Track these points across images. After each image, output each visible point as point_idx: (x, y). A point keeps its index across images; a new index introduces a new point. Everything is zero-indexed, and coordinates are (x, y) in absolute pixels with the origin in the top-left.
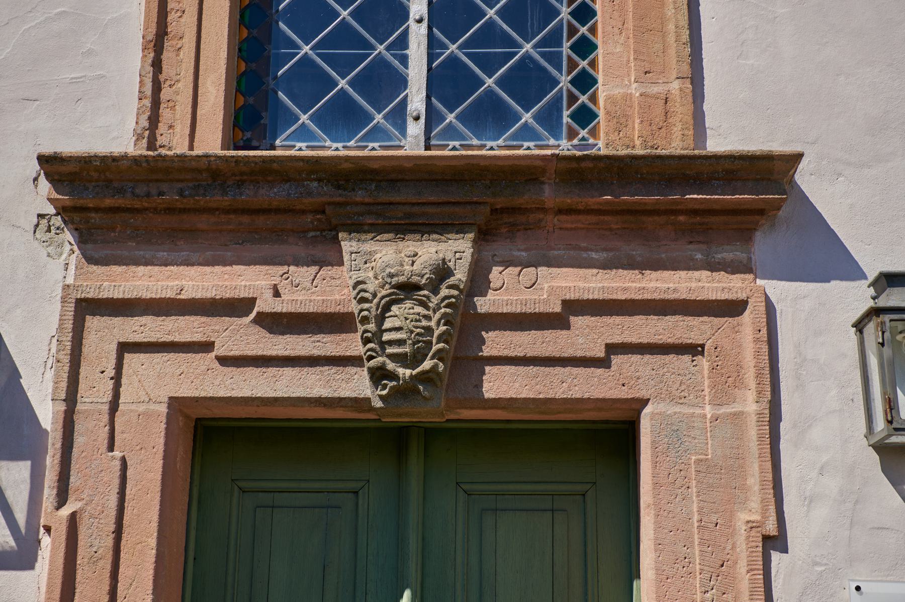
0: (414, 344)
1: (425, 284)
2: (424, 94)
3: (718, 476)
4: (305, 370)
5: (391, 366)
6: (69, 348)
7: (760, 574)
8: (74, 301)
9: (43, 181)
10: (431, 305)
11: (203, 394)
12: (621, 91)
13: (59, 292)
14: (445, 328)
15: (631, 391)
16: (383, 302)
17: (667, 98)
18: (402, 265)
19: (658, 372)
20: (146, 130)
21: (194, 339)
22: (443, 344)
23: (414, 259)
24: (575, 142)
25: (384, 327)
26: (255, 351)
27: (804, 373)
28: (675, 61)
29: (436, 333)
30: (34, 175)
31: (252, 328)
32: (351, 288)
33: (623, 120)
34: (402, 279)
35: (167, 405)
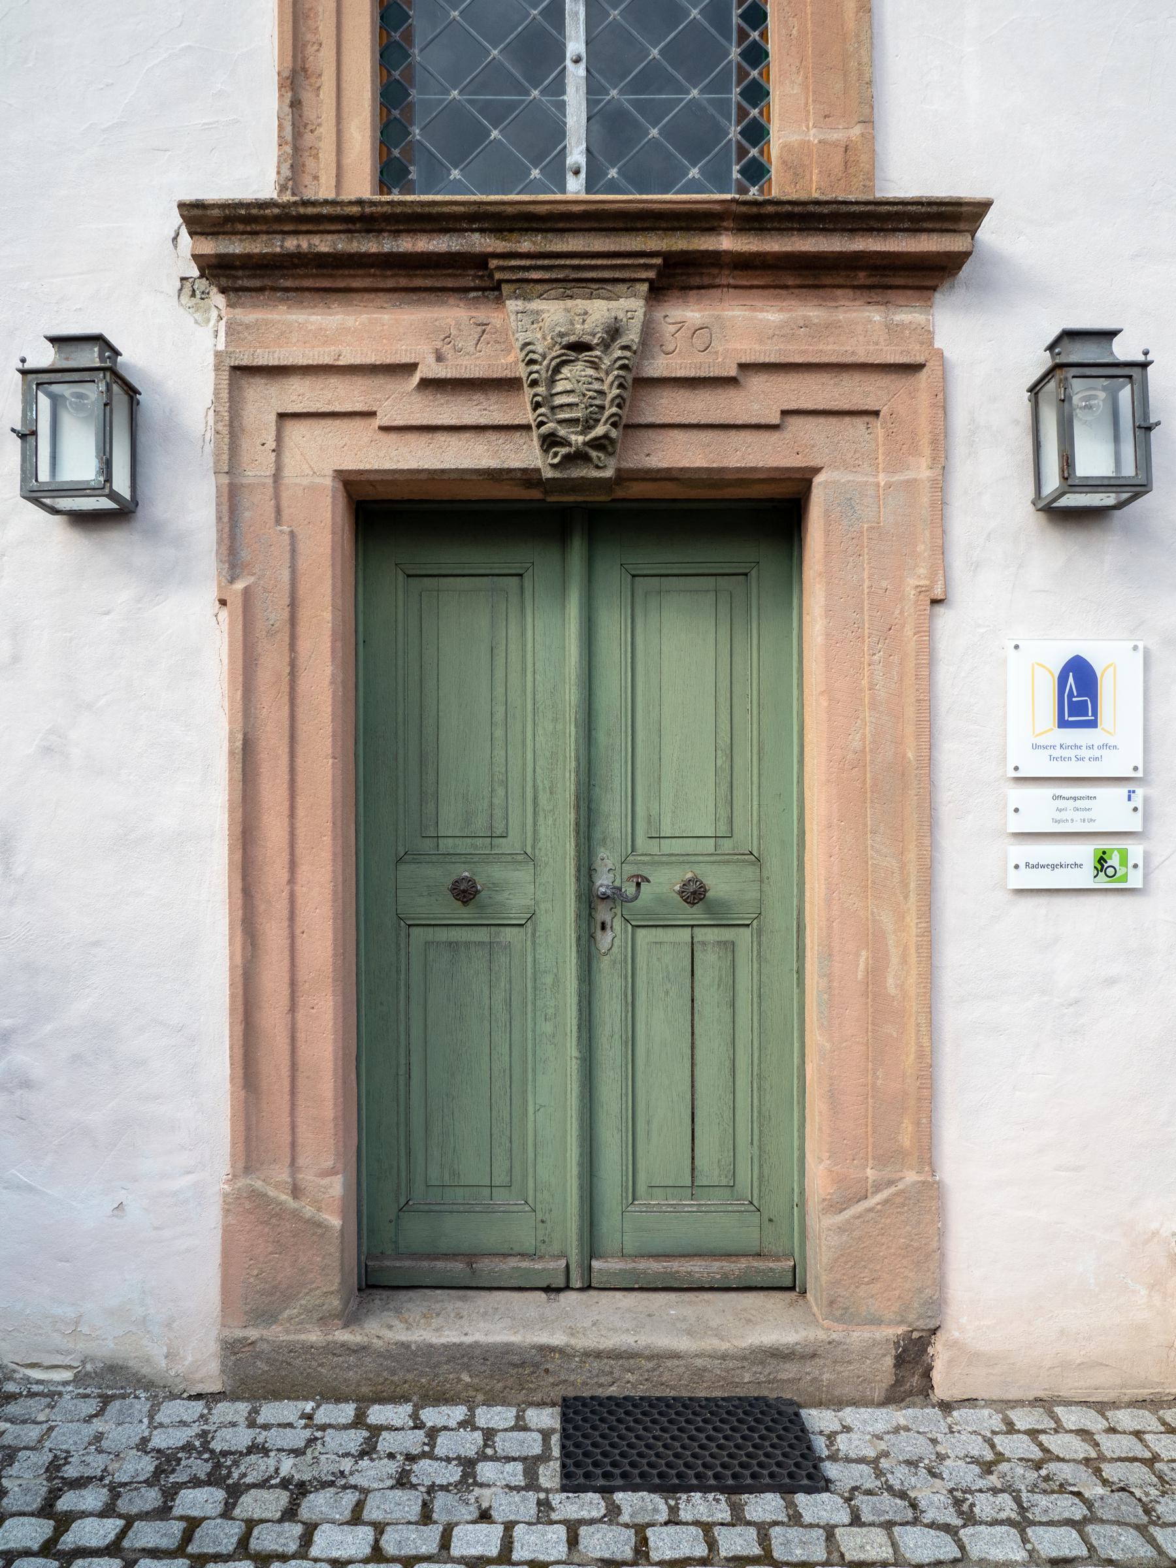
1: (598, 344)
2: (584, 145)
5: (562, 432)
6: (227, 418)
10: (603, 366)
11: (368, 467)
12: (799, 138)
13: (210, 360)
14: (618, 391)
16: (553, 363)
18: (573, 324)
23: (585, 317)
25: (554, 391)
30: (173, 235)
32: (519, 351)
33: (801, 170)
34: (573, 339)
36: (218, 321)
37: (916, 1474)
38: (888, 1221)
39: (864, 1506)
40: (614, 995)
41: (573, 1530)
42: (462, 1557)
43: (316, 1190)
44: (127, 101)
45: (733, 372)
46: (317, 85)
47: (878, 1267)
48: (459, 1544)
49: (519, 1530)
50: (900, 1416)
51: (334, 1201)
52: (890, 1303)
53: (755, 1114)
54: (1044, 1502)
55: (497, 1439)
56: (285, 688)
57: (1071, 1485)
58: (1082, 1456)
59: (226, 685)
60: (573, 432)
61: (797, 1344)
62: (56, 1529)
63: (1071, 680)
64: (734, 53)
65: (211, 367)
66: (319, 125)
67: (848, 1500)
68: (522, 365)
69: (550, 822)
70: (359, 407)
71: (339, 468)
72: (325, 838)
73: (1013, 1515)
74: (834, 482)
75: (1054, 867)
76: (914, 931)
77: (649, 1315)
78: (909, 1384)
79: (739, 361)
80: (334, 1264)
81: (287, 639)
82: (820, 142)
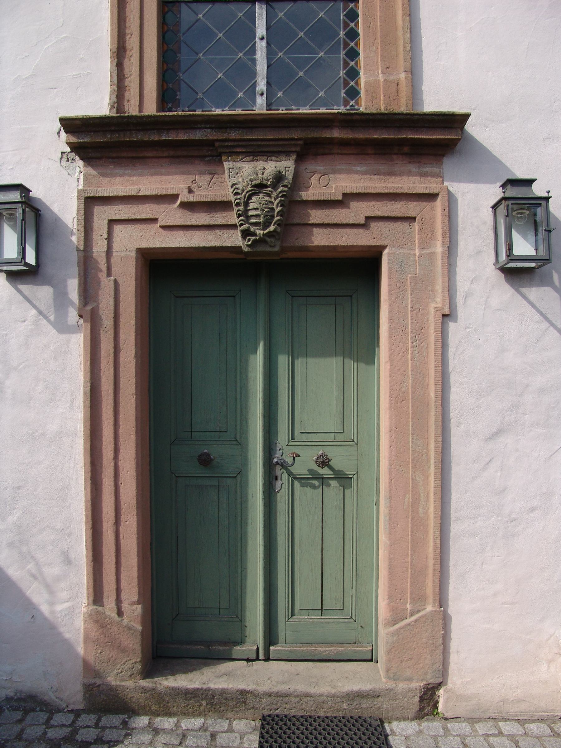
0: (264, 217)
1: (270, 185)
3: (421, 285)
4: (207, 232)
7: (440, 333)
8: (84, 198)
9: (63, 133)
11: (154, 246)
12: (374, 78)
13: (75, 194)
14: (281, 208)
15: (378, 241)
16: (247, 195)
17: (398, 83)
18: (257, 175)
19: (392, 232)
20: (115, 103)
21: (148, 217)
22: (280, 217)
23: (264, 171)
24: (348, 107)
25: (249, 208)
26: (180, 223)
27: (466, 232)
28: (403, 62)
29: (276, 211)
30: (58, 130)
31: (178, 210)
34: (257, 182)
35: (135, 252)
36: (80, 174)
43: (129, 611)
44: (36, 64)
45: (340, 198)
47: (412, 653)
52: (417, 670)
59: (82, 358)
60: (258, 229)
61: (370, 690)
64: (342, 34)
65: (76, 197)
66: (131, 75)
68: (232, 195)
70: (149, 216)
72: (132, 436)
78: (426, 710)
79: (343, 192)
81: (113, 335)
82: (384, 81)
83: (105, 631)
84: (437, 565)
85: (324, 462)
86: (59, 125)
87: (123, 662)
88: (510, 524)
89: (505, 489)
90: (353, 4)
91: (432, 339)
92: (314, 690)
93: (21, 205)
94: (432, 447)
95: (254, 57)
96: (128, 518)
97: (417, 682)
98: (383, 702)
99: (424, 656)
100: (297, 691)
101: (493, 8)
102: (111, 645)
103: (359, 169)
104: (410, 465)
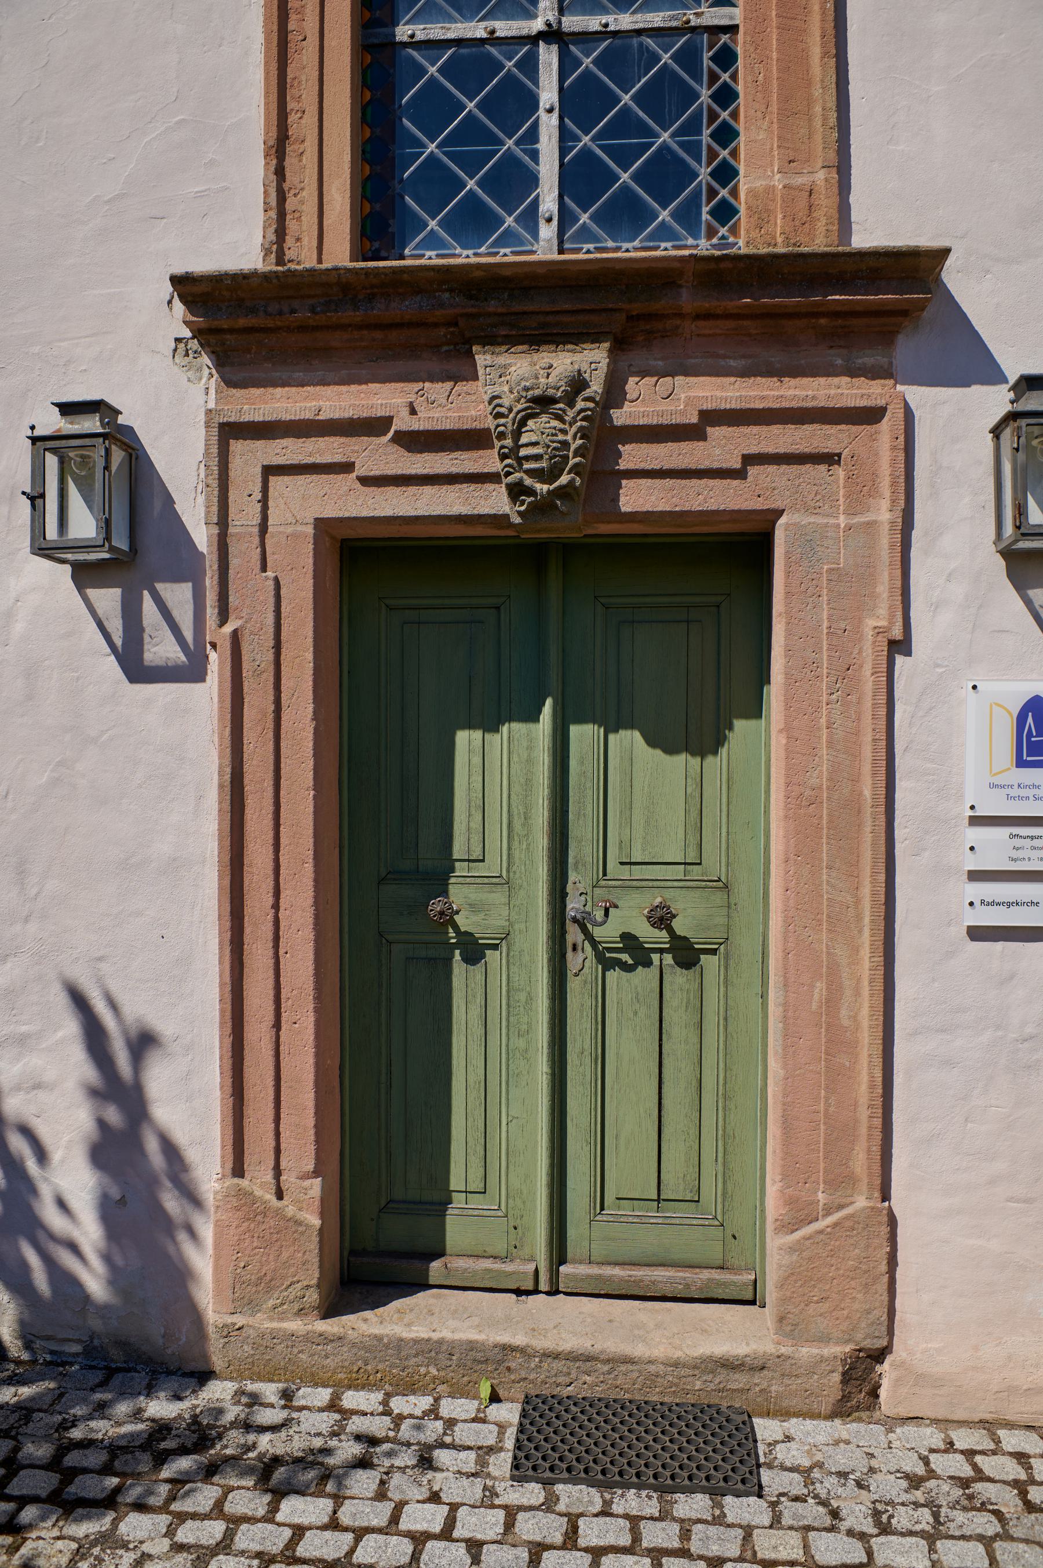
1: (560, 397)
5: (528, 481)
11: (347, 515)
12: (764, 183)
13: (202, 417)
14: (581, 441)
16: (519, 416)
17: (811, 190)
18: (537, 378)
23: (550, 371)
24: (715, 241)
26: (394, 471)
29: (573, 447)
30: (168, 298)
32: (486, 403)
34: (537, 392)
36: (209, 379)
37: (844, 1485)
38: (837, 1243)
39: (786, 1511)
40: (585, 1013)
41: (511, 1513)
42: (409, 1532)
43: (298, 1191)
46: (301, 151)
47: (828, 1287)
48: (407, 1519)
49: (462, 1512)
50: (839, 1428)
51: (314, 1201)
52: (838, 1322)
53: (720, 1132)
54: (961, 1518)
55: (456, 1429)
56: (270, 724)
57: (992, 1504)
58: (1011, 1477)
59: (216, 722)
61: (746, 1356)
62: (61, 1482)
63: (1030, 720)
65: (202, 423)
66: (302, 189)
67: (773, 1505)
68: (490, 417)
69: (524, 846)
71: (321, 516)
72: (307, 865)
73: (928, 1528)
74: (794, 524)
75: (1009, 905)
76: (867, 965)
77: (610, 1321)
78: (855, 1400)
80: (314, 1260)
82: (784, 187)
83: (252, 1225)
84: (875, 1119)
85: (662, 918)
86: (171, 289)
87: (284, 1286)
88: (1021, 1046)
89: (1012, 977)
90: (728, 35)
91: (868, 687)
92: (639, 1350)
93: (101, 440)
94: (866, 891)
95: (535, 146)
96: (298, 1017)
97: (837, 1343)
98: (772, 1379)
99: (851, 1294)
100: (608, 1350)
101: (1003, 36)
102: (263, 1252)
103: (732, 363)
104: (824, 927)
